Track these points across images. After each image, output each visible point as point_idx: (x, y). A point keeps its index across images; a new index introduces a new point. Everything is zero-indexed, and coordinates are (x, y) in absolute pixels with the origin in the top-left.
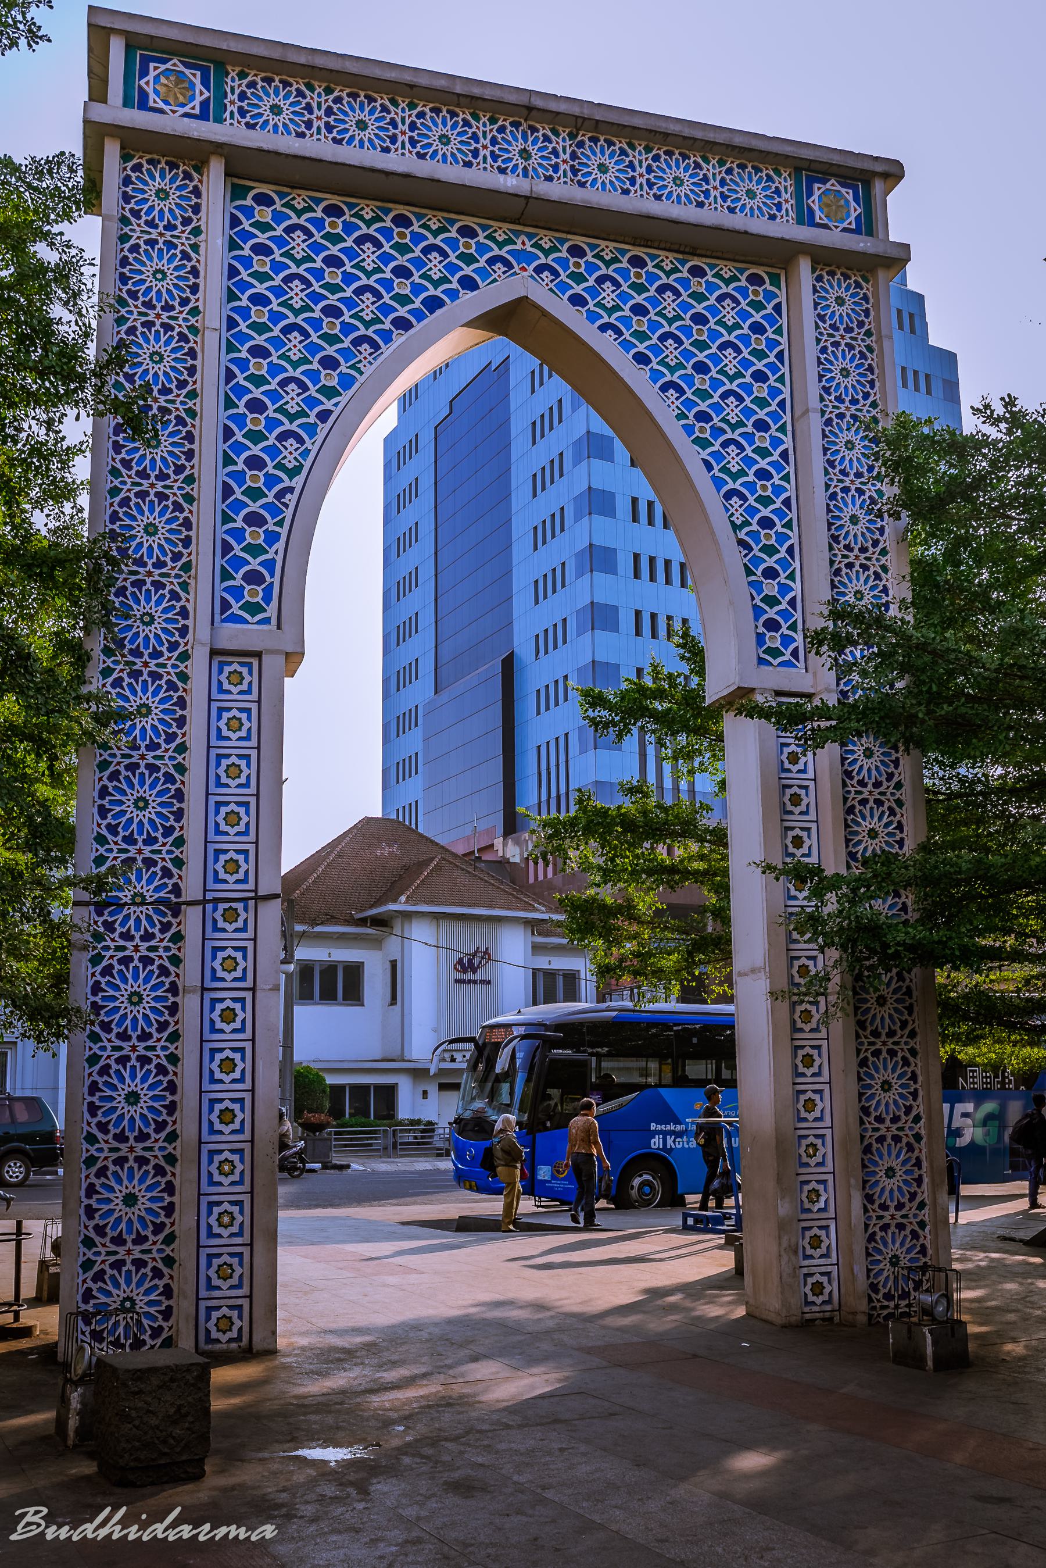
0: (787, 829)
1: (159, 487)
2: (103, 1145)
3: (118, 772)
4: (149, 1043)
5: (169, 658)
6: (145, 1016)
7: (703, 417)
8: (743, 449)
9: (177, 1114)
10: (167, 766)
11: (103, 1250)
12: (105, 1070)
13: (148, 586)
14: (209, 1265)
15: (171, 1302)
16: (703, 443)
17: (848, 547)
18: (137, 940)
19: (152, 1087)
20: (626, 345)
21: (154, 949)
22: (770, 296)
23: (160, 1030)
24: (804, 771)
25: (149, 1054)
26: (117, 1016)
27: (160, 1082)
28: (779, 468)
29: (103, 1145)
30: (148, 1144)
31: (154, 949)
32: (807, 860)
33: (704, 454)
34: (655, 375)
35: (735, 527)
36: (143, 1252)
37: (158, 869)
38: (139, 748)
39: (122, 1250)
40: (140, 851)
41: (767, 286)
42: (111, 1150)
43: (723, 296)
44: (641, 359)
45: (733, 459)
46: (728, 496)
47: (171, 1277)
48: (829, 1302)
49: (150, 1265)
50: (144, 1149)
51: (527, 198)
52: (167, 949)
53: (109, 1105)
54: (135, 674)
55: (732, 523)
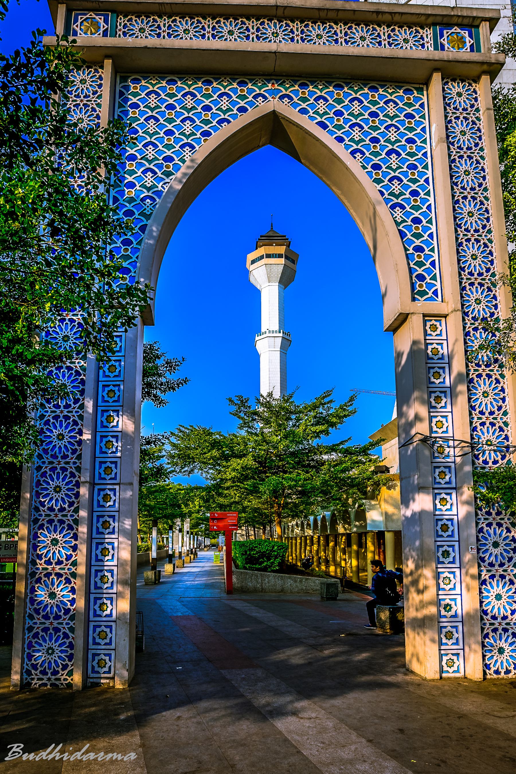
0: (436, 467)
1: (55, 623)
2: (48, 409)
3: (49, 420)
4: (64, 513)
5: (72, 458)
6: (55, 661)
7: (376, 167)
8: (398, 129)
9: (78, 551)
10: (69, 520)
11: (49, 410)
12: (47, 423)
13: (56, 522)
14: (98, 521)
15: (73, 651)
16: (378, 181)
17: (467, 230)
18: (59, 458)
19: (73, 382)
20: (331, 133)
21: (67, 463)
22: (417, 99)
23: (73, 454)
24: (440, 335)
25: (64, 519)
26: (51, 446)
27: (77, 379)
28: (428, 244)
29: (48, 409)
30: (70, 409)
31: (67, 463)
32: (457, 675)
33: (379, 187)
34: (347, 147)
35: (397, 224)
36: (58, 623)
37: (68, 473)
38: (57, 458)
39: (58, 411)
40: (51, 623)
41: (416, 94)
42: (52, 412)
43: (390, 102)
44: (340, 140)
45: (396, 187)
46: (393, 207)
47: (82, 425)
48: (458, 671)
49: (73, 405)
50: (68, 412)
51: (275, 52)
52: (75, 463)
53: (49, 440)
54: (53, 469)
55: (395, 221)
